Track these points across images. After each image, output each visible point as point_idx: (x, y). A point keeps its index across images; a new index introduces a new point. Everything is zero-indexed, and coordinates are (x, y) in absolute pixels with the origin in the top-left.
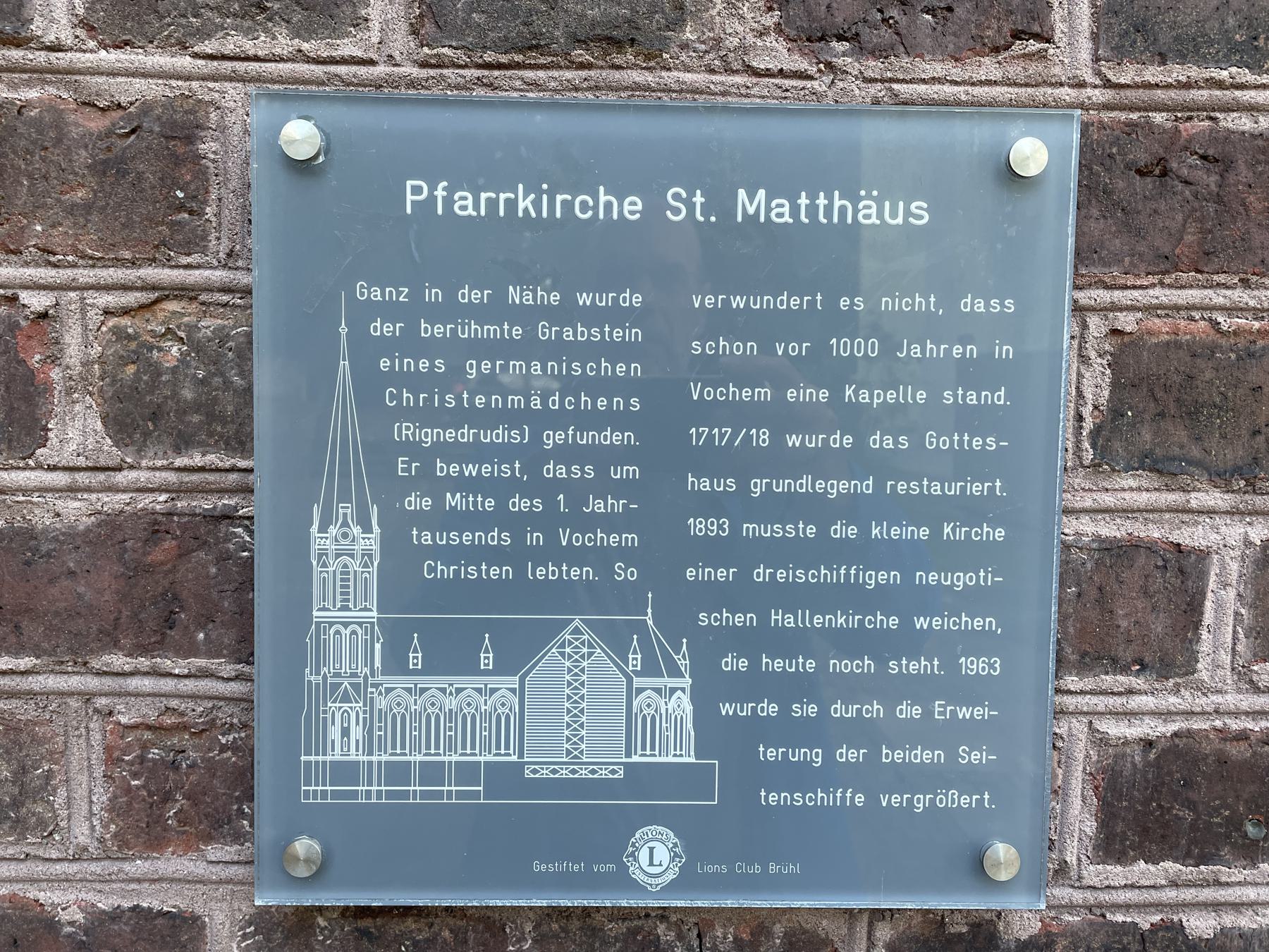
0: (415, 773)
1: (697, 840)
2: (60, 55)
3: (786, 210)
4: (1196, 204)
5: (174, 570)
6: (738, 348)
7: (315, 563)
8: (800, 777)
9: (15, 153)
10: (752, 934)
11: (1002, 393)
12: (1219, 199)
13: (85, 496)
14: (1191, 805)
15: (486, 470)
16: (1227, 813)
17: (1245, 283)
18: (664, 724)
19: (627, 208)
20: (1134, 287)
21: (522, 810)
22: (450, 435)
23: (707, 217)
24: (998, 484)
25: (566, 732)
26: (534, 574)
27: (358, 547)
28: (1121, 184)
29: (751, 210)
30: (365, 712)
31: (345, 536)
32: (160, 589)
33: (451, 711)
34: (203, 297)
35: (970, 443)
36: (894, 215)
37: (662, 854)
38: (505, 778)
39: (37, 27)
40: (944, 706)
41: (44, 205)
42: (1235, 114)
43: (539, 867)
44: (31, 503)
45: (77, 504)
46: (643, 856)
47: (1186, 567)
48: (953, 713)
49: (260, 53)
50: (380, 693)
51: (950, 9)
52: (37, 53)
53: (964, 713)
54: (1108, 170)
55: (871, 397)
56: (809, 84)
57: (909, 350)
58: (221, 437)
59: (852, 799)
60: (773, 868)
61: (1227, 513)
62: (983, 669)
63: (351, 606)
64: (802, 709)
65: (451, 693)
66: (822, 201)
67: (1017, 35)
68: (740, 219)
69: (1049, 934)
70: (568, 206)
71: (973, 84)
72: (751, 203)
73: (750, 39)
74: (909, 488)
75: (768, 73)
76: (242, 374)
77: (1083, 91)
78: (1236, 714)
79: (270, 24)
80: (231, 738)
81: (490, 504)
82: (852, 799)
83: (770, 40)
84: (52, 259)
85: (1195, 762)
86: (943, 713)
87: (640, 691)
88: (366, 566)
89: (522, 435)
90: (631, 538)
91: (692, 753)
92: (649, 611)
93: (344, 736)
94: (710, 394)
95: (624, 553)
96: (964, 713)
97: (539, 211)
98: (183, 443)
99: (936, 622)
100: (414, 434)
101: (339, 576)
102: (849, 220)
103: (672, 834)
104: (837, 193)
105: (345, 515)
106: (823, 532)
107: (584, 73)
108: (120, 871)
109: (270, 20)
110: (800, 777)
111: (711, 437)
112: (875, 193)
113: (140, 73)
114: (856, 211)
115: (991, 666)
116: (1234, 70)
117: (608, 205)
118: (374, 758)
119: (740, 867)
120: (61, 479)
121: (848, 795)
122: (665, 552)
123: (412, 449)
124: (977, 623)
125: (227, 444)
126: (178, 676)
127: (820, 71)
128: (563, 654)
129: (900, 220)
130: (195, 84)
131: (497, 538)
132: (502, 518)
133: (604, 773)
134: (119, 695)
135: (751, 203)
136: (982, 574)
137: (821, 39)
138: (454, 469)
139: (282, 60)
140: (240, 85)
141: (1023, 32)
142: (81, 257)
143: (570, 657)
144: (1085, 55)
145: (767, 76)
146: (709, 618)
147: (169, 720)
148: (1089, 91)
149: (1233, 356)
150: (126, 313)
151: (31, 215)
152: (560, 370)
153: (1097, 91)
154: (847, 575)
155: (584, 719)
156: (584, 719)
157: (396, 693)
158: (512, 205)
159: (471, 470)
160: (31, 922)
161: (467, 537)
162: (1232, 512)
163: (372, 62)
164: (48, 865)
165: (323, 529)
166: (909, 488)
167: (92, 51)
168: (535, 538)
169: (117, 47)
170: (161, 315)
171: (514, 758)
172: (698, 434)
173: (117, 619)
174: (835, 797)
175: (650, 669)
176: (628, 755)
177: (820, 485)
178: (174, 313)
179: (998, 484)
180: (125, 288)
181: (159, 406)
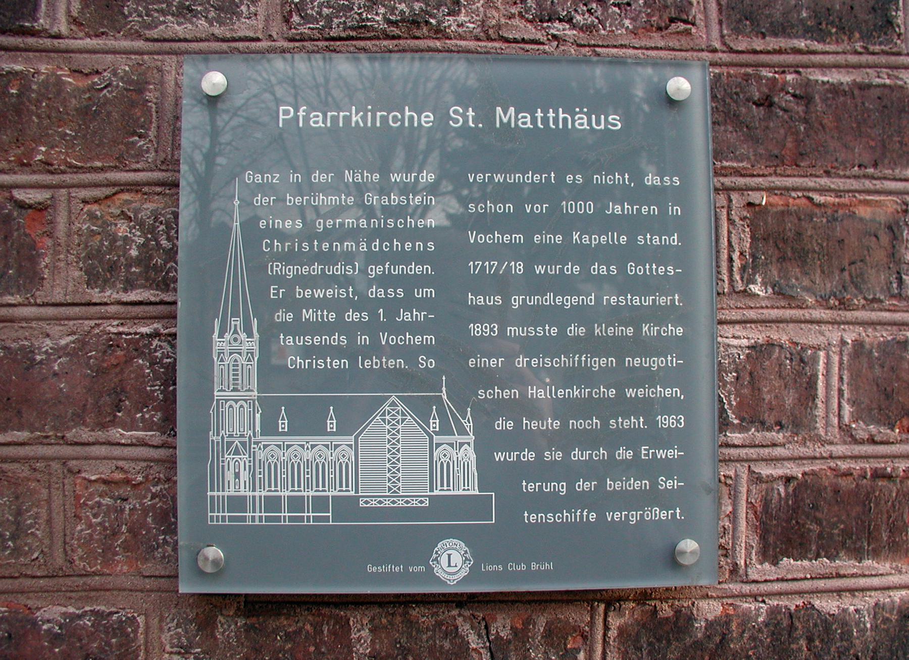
0: (285, 504)
1: (480, 546)
2: (60, 41)
3: (528, 119)
4: (792, 124)
5: (122, 372)
6: (500, 208)
7: (215, 359)
8: (551, 503)
9: (30, 101)
10: (523, 624)
11: (676, 238)
12: (806, 121)
13: (66, 322)
14: (818, 522)
15: (329, 293)
16: (842, 526)
17: (827, 173)
18: (456, 468)
19: (423, 119)
20: (759, 176)
21: (357, 525)
22: (305, 270)
23: (476, 125)
24: (677, 297)
25: (388, 475)
26: (363, 364)
27: (244, 348)
28: (743, 110)
29: (505, 120)
30: (250, 462)
31: (235, 340)
32: (113, 385)
33: (308, 460)
34: (145, 189)
35: (657, 270)
36: (598, 123)
37: (457, 559)
38: (346, 507)
39: (42, 22)
40: (648, 450)
41: (47, 135)
42: (812, 70)
43: (371, 569)
44: (31, 328)
45: (61, 328)
46: (444, 560)
47: (802, 359)
48: (654, 454)
49: (187, 37)
50: (260, 449)
51: (629, 4)
52: (46, 40)
53: (661, 454)
54: (736, 102)
55: (590, 240)
56: (541, 47)
57: (613, 209)
58: (154, 281)
59: (588, 516)
60: (534, 566)
61: (829, 323)
62: (673, 423)
63: (239, 388)
64: (551, 455)
65: (308, 448)
66: (551, 114)
67: (672, 20)
68: (498, 125)
69: (727, 615)
70: (384, 119)
71: (647, 49)
72: (505, 115)
73: (503, 21)
74: (618, 301)
75: (515, 41)
76: (169, 239)
77: (716, 54)
78: (843, 458)
79: (195, 19)
80: (159, 488)
81: (332, 316)
82: (588, 516)
83: (517, 22)
84: (51, 168)
85: (819, 491)
86: (647, 455)
87: (438, 445)
88: (249, 360)
89: (354, 269)
90: (430, 339)
91: (476, 488)
92: (444, 389)
93: (236, 479)
94: (482, 238)
95: (426, 350)
96: (661, 454)
97: (365, 123)
98: (129, 285)
99: (641, 392)
100: (281, 270)
101: (231, 368)
102: (570, 127)
103: (463, 544)
104: (561, 110)
105: (235, 326)
106: (562, 332)
107: (395, 42)
108: (84, 583)
109: (195, 17)
110: (551, 503)
111: (483, 268)
112: (585, 110)
113: (113, 56)
114: (573, 121)
115: (678, 421)
116: (808, 42)
117: (411, 118)
118: (257, 494)
119: (512, 567)
120: (51, 311)
121: (585, 513)
122: (454, 348)
123: (280, 280)
124: (668, 392)
125: (158, 285)
126: (124, 445)
127: (548, 39)
128: (384, 420)
129: (602, 127)
130: (146, 57)
131: (338, 339)
132: (340, 326)
133: (415, 503)
134: (86, 458)
135: (505, 115)
136: (669, 358)
137: (549, 21)
138: (308, 293)
139: (201, 40)
140: (174, 57)
141: (676, 18)
142: (70, 167)
143: (389, 422)
144: (715, 33)
145: (514, 42)
146: (485, 393)
147: (119, 476)
148: (720, 55)
149: (824, 220)
150: (96, 202)
151: (38, 141)
152: (380, 224)
153: (725, 55)
154: (580, 361)
155: (400, 465)
156: (400, 465)
157: (271, 450)
158: (347, 119)
159: (319, 294)
160: (21, 621)
161: (317, 340)
162: (833, 323)
163: (258, 40)
164: (34, 580)
165: (221, 335)
166: (618, 301)
167: (81, 39)
168: (363, 339)
169: (97, 36)
170: (118, 203)
171: (352, 493)
172: (474, 266)
173: (85, 405)
174: (576, 516)
175: (445, 430)
176: (431, 490)
177: (559, 299)
178: (126, 201)
179: (677, 297)
180: (96, 185)
181: (115, 262)
